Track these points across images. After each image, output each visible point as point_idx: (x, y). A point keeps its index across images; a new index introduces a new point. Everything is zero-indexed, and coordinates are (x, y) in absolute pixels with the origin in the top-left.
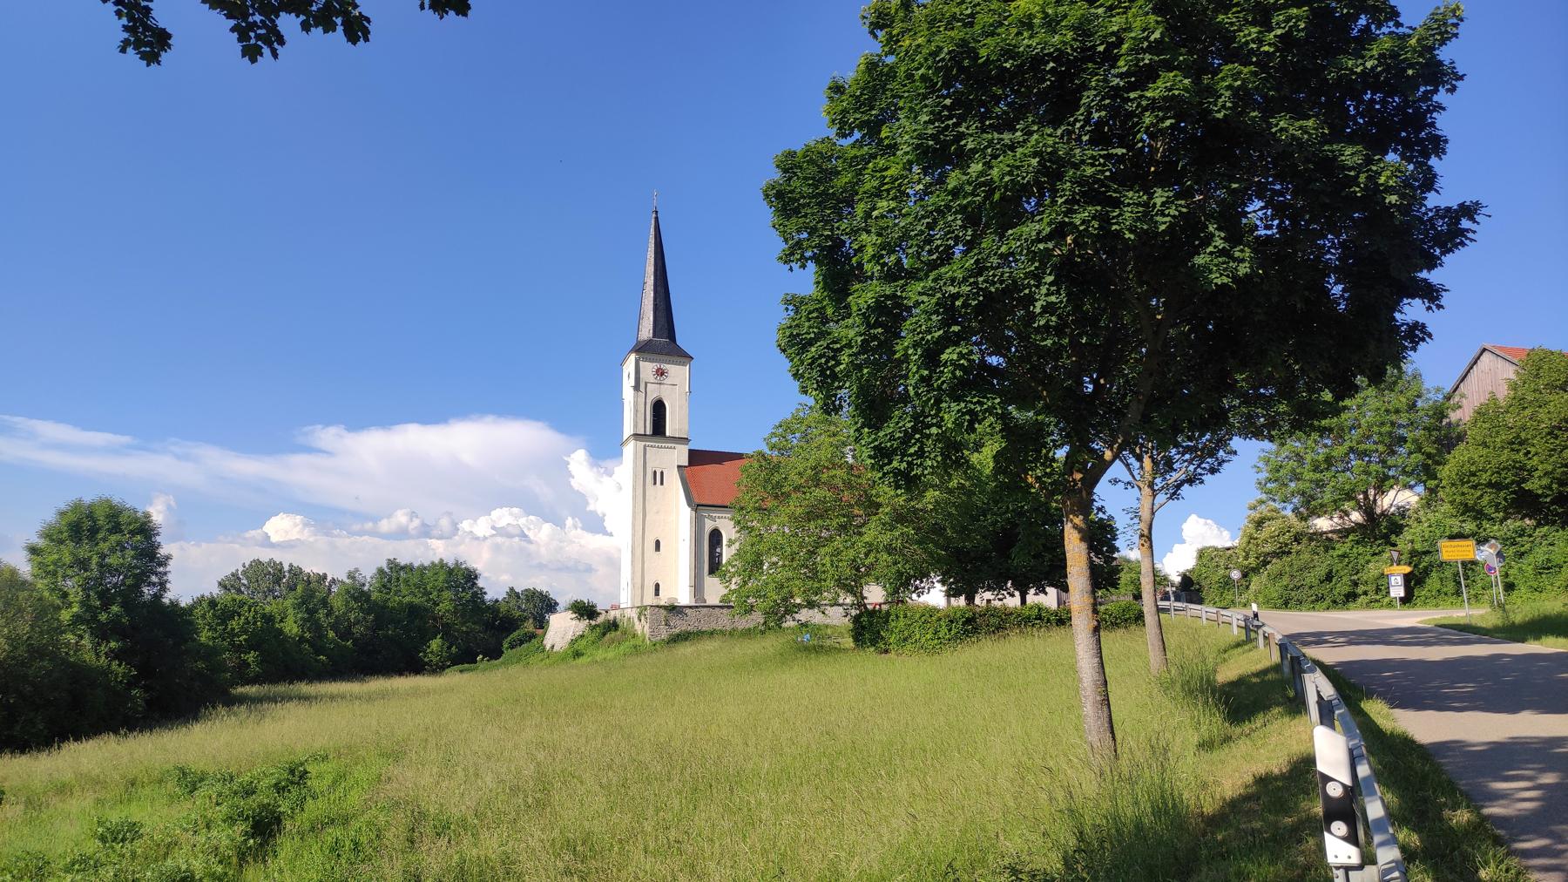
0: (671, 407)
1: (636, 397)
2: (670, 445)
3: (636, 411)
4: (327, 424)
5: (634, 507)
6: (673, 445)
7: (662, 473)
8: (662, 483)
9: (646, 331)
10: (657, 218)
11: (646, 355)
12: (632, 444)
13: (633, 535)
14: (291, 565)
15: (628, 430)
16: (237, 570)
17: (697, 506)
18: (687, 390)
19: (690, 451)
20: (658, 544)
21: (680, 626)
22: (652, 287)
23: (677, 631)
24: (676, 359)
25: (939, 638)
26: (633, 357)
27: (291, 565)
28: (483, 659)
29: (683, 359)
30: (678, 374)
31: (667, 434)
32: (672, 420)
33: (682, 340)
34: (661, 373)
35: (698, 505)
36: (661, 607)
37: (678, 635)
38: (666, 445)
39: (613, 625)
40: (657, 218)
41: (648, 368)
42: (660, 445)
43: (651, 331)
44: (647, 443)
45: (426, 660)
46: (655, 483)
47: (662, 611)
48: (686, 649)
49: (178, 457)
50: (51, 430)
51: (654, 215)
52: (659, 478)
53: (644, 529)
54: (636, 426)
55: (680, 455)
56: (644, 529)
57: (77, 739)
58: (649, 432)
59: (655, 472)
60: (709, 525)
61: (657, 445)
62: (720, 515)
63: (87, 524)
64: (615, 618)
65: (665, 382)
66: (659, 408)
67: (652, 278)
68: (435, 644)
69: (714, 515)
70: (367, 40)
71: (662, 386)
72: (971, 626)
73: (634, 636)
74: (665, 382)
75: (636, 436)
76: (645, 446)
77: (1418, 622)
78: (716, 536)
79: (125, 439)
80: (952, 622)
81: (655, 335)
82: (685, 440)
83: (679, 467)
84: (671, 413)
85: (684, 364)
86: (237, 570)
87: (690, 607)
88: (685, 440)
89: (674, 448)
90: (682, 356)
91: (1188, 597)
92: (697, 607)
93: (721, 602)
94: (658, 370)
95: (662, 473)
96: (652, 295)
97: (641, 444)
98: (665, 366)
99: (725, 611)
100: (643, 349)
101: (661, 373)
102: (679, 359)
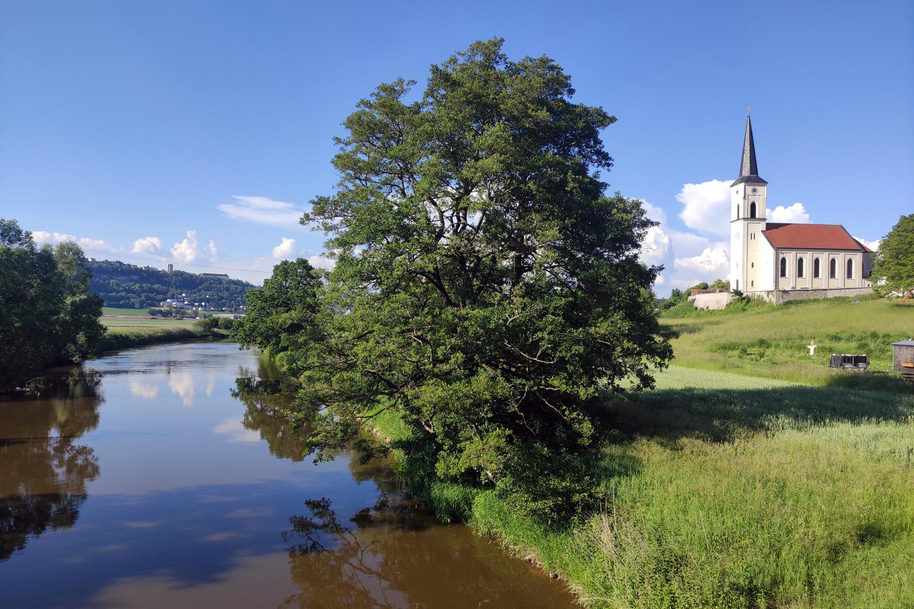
0: (759, 205)
1: (744, 202)
3: (744, 208)
9: (746, 172)
13: (743, 261)
17: (777, 249)
21: (787, 298)
23: (786, 300)
24: (761, 184)
30: (762, 190)
31: (757, 217)
32: (759, 211)
33: (761, 175)
34: (754, 190)
39: (749, 300)
48: (793, 308)
50: (259, 201)
52: (753, 236)
54: (744, 215)
55: (762, 226)
57: (260, 196)
58: (749, 217)
60: (781, 256)
66: (753, 206)
70: (333, 162)
73: (766, 302)
75: (745, 219)
79: (290, 205)
81: (751, 174)
83: (762, 231)
84: (759, 207)
85: (764, 186)
90: (763, 182)
97: (746, 222)
98: (757, 188)
100: (747, 181)
101: (754, 190)
102: (762, 184)
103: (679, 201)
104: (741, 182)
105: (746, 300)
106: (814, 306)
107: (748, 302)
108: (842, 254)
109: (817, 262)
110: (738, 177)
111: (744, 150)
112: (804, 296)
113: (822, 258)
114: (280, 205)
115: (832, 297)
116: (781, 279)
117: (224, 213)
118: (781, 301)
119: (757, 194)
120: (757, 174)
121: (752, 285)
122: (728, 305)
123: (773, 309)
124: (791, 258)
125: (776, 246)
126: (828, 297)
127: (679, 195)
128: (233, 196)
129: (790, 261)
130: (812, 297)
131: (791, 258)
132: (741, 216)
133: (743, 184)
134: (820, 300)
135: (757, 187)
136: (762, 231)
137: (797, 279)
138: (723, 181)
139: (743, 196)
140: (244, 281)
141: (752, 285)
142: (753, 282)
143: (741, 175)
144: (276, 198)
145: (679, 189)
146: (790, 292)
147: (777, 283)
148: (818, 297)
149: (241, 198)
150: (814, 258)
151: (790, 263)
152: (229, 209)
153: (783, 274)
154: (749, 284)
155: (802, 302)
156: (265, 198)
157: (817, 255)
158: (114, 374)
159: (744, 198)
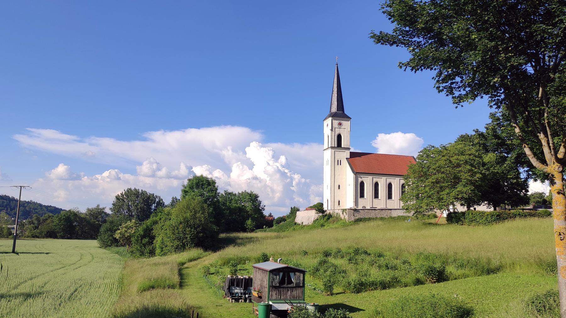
0: (344, 136)
1: (331, 133)
2: (343, 151)
3: (332, 138)
4: (157, 129)
5: (331, 173)
6: (344, 151)
7: (340, 161)
8: (340, 165)
9: (334, 109)
10: (337, 67)
11: (335, 118)
12: (330, 150)
14: (142, 190)
15: (326, 146)
16: (122, 192)
18: (349, 130)
19: (350, 152)
20: (339, 186)
21: (358, 216)
22: (336, 93)
23: (357, 218)
25: (488, 221)
26: (330, 119)
27: (142, 190)
28: (266, 227)
29: (348, 119)
30: (346, 124)
31: (342, 146)
32: (344, 141)
33: (346, 112)
34: (340, 124)
35: (356, 173)
36: (352, 209)
37: (358, 219)
38: (342, 151)
39: (330, 216)
40: (337, 67)
41: (336, 122)
42: (340, 150)
43: (336, 109)
44: (336, 150)
45: (247, 227)
46: (338, 164)
47: (352, 211)
48: (361, 224)
49: (91, 144)
51: (336, 66)
52: (339, 163)
53: (334, 181)
54: (331, 144)
55: (347, 154)
56: (334, 181)
58: (336, 146)
59: (338, 161)
60: (360, 180)
61: (339, 150)
62: (364, 176)
63: (201, 183)
64: (330, 213)
65: (341, 127)
66: (339, 137)
67: (336, 89)
68: (249, 222)
69: (362, 176)
71: (340, 129)
72: (499, 218)
73: (341, 219)
74: (341, 127)
75: (332, 148)
76: (335, 151)
77: (257, 240)
78: (362, 184)
79: (74, 137)
80: (492, 216)
82: (349, 149)
85: (348, 121)
86: (122, 192)
87: (361, 210)
88: (349, 149)
89: (345, 152)
90: (347, 118)
91: (545, 207)
92: (364, 210)
93: (363, 207)
94: (339, 123)
95: (340, 161)
96: (336, 96)
99: (373, 211)
100: (334, 116)
101: (340, 124)
103: (374, 146)
104: (329, 117)
105: (327, 217)
106: (372, 224)
107: (329, 219)
108: (397, 179)
109: (390, 186)
110: (329, 113)
111: (333, 91)
112: (372, 214)
113: (394, 183)
114: (66, 137)
115: (396, 216)
116: (360, 200)
117: (17, 141)
118: (353, 219)
119: (342, 127)
120: (343, 111)
121: (339, 204)
122: (315, 221)
123: (345, 225)
124: (368, 182)
125: (356, 171)
126: (393, 216)
127: (374, 141)
128: (28, 129)
129: (367, 184)
130: (379, 216)
131: (368, 182)
132: (330, 146)
133: (330, 119)
134: (385, 219)
135: (342, 122)
136: (347, 158)
137: (388, 201)
138: (405, 133)
139: (331, 129)
140: (10, 197)
141: (339, 204)
142: (339, 202)
143: (330, 111)
144: (64, 132)
145: (375, 137)
146: (361, 211)
147: (356, 203)
148: (384, 216)
149: (33, 130)
150: (388, 183)
151: (367, 186)
152: (23, 140)
153: (362, 196)
154: (337, 203)
155: (369, 219)
156: (54, 131)
157: (390, 180)
158: (264, 269)
159: (332, 130)
